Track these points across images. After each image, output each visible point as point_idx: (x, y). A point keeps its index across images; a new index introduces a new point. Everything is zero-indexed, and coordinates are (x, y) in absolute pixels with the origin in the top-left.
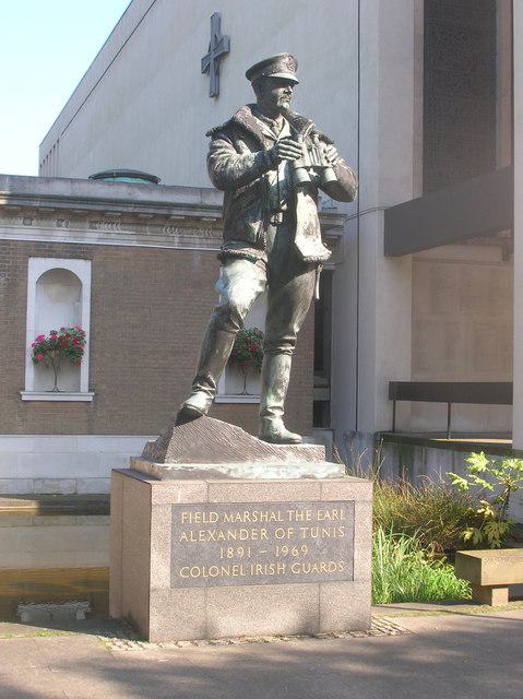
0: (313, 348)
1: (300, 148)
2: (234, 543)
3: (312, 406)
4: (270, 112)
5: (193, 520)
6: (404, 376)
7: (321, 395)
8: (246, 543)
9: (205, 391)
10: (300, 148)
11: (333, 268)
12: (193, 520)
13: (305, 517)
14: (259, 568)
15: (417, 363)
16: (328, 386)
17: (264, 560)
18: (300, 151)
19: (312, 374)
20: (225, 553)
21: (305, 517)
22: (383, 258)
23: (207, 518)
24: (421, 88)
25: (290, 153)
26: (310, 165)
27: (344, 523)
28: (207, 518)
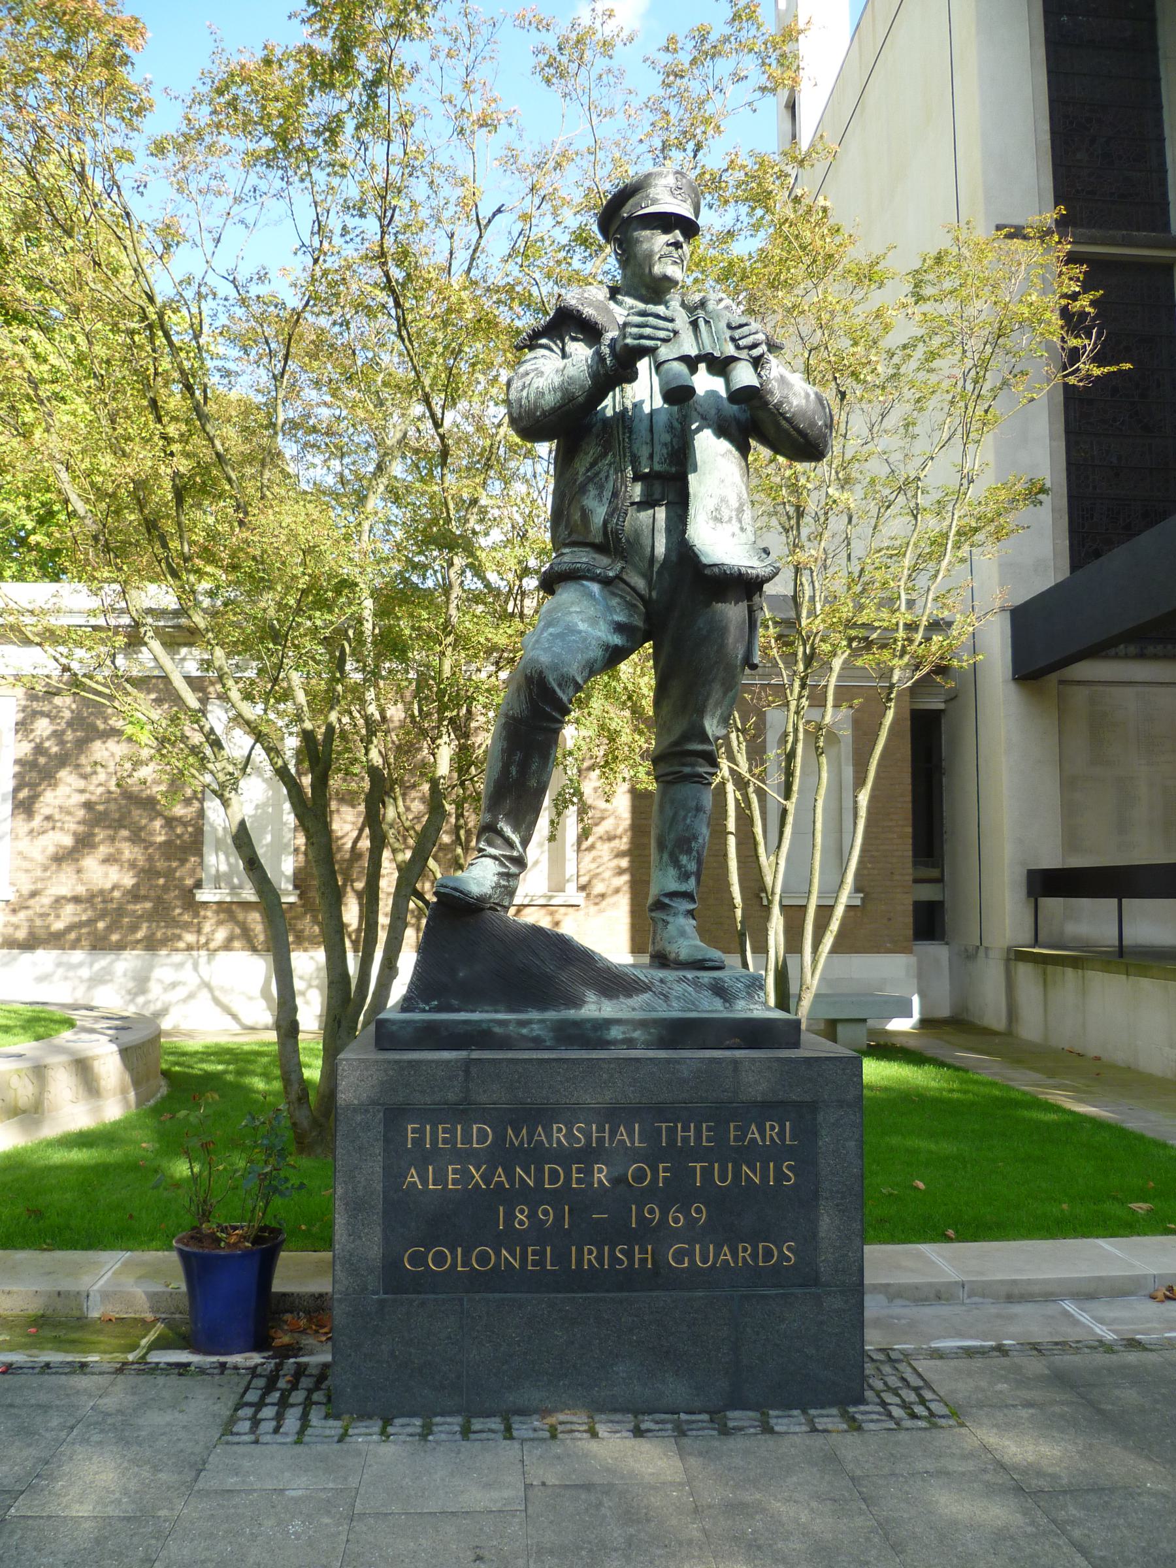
0: (910, 822)
1: (672, 320)
2: (532, 1197)
3: (911, 908)
4: (644, 292)
5: (434, 1141)
6: (1051, 859)
7: (927, 893)
8: (556, 1198)
9: (495, 858)
10: (672, 320)
11: (942, 706)
12: (434, 1141)
13: (699, 1136)
14: (590, 1255)
15: (1071, 840)
16: (940, 880)
17: (602, 1236)
18: (669, 325)
19: (910, 865)
20: (510, 1216)
21: (699, 1136)
22: (1012, 687)
23: (467, 1138)
24: (1060, 426)
25: (647, 331)
26: (693, 352)
27: (790, 1152)
28: (467, 1138)
